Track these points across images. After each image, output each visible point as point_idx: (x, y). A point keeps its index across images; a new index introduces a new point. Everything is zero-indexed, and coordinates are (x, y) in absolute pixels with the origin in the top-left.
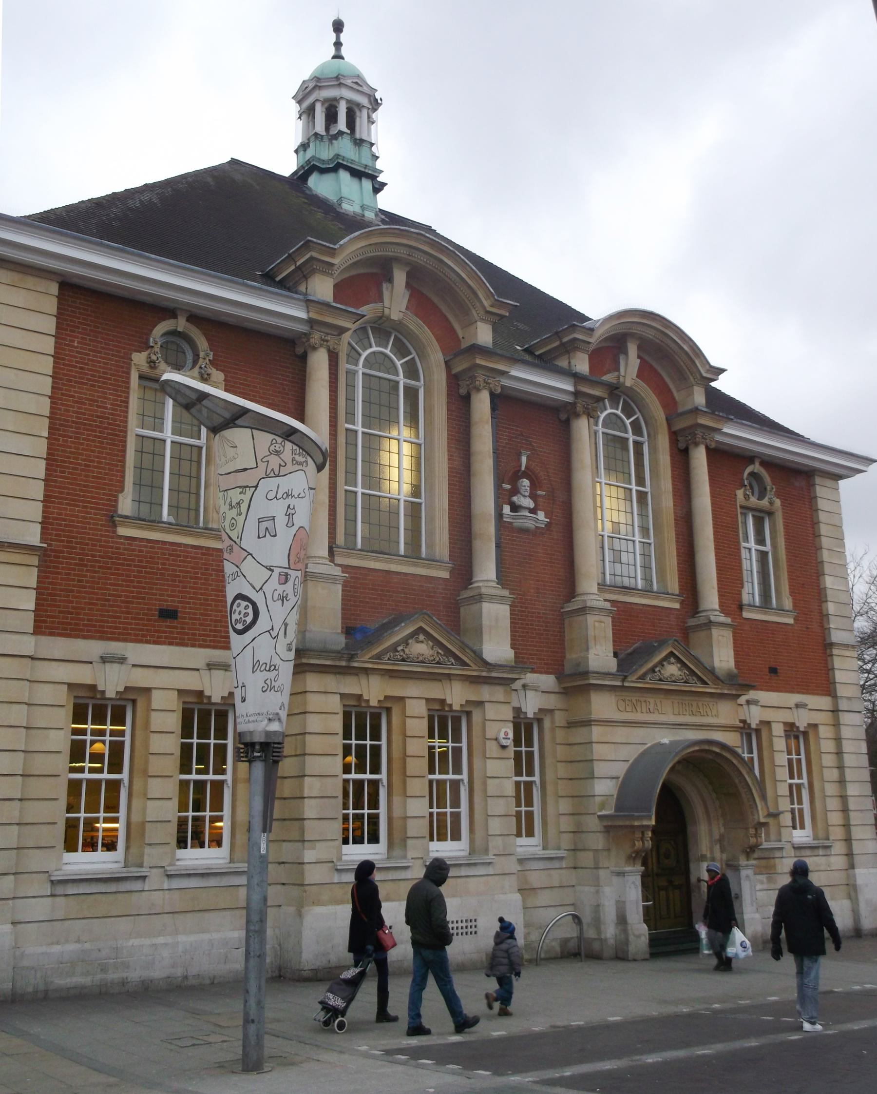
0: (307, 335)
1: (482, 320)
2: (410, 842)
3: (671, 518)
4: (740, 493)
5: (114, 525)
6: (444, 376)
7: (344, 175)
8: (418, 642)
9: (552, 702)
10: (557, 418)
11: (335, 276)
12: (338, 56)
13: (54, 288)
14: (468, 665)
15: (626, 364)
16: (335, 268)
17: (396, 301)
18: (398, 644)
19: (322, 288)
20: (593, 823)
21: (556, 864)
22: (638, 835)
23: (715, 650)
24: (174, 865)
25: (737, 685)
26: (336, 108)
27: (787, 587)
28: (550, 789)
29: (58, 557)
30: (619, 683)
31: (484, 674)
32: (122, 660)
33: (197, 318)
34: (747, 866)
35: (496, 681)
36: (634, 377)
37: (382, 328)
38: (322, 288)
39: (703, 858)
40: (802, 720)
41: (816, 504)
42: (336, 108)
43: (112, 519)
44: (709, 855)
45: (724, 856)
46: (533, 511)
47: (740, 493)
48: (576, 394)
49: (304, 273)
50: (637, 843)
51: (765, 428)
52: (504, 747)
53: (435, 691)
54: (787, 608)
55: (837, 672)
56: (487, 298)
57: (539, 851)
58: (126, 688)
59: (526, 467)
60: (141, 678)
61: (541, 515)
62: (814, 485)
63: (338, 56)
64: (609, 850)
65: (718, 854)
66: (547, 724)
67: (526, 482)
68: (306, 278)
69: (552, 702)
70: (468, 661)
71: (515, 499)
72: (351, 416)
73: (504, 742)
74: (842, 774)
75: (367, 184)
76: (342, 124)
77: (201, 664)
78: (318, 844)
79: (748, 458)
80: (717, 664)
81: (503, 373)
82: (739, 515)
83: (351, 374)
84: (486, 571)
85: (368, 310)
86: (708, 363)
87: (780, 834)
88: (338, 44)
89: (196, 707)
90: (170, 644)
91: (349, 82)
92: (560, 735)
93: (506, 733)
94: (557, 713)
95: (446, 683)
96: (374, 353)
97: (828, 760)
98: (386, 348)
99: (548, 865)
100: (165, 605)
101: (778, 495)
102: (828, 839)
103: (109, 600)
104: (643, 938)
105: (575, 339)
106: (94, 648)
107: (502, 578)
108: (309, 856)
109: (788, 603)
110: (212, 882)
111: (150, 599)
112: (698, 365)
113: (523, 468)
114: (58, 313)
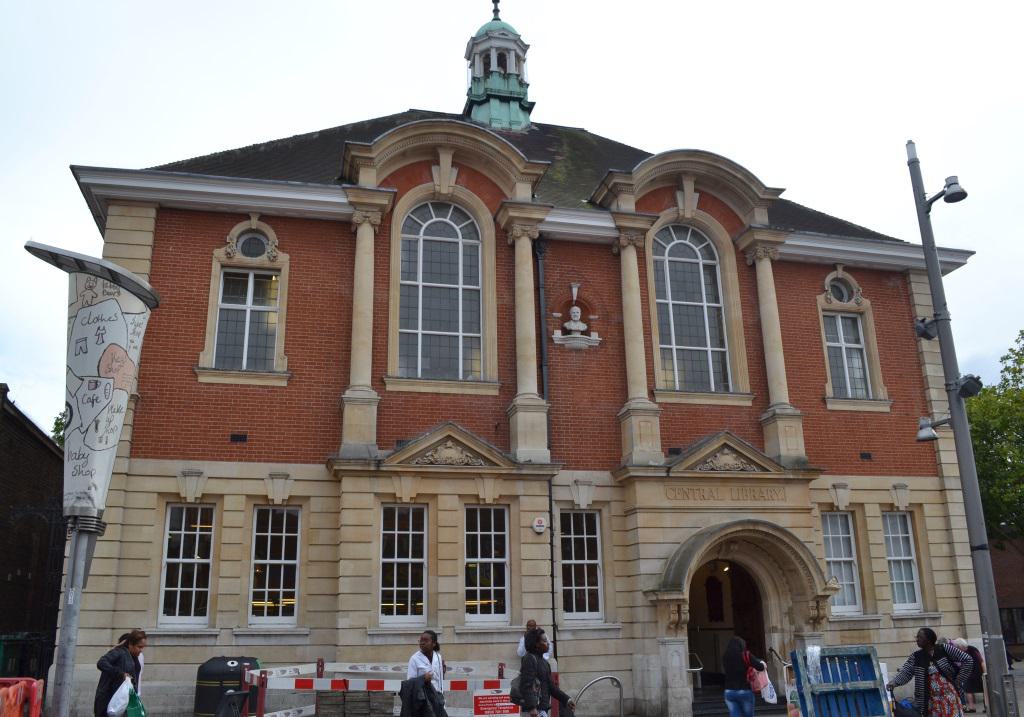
0: (618, 239)
1: (520, 181)
2: (441, 614)
3: (741, 330)
4: (821, 299)
5: (196, 375)
6: (493, 232)
7: (494, 103)
8: (447, 448)
9: (606, 494)
10: (607, 252)
11: (636, 193)
12: (496, 19)
13: (152, 213)
14: (768, 470)
15: (440, 175)
16: (376, 160)
17: (688, 203)
18: (427, 449)
19: (627, 203)
20: (640, 599)
21: (612, 635)
22: (674, 608)
23: (781, 439)
24: (378, 626)
25: (805, 471)
26: (496, 57)
27: (881, 374)
28: (608, 568)
29: (152, 402)
30: (664, 474)
31: (514, 472)
32: (199, 474)
33: (265, 217)
34: (811, 636)
35: (431, 476)
36: (695, 209)
37: (680, 227)
38: (627, 203)
39: (774, 629)
40: (902, 500)
41: (913, 300)
42: (496, 57)
43: (194, 370)
44: (779, 627)
45: (793, 628)
46: (586, 333)
47: (821, 299)
48: (619, 228)
49: (614, 193)
50: (672, 616)
51: (310, 184)
52: (539, 534)
53: (468, 487)
54: (882, 398)
55: (942, 453)
56: (520, 162)
57: (600, 624)
58: (203, 495)
59: (578, 297)
60: (215, 488)
61: (595, 336)
62: (910, 282)
63: (496, 19)
64: (656, 622)
65: (787, 626)
66: (605, 513)
67: (576, 311)
68: (616, 196)
69: (606, 494)
70: (498, 462)
71: (566, 325)
72: (661, 293)
73: (538, 529)
74: (952, 549)
75: (515, 106)
76: (494, 66)
77: (889, 486)
78: (351, 614)
79: (824, 267)
80: (783, 451)
81: (541, 221)
82: (821, 318)
83: (659, 265)
84: (528, 384)
85: (666, 216)
86: (763, 185)
87: (876, 607)
88: (496, 11)
89: (572, 513)
90: (241, 460)
91: (496, 34)
92: (616, 522)
93: (540, 522)
94: (612, 504)
95: (479, 481)
96: (677, 244)
97: (936, 537)
98: (686, 239)
99: (604, 635)
100: (236, 432)
101: (864, 295)
102: (937, 611)
103: (191, 431)
104: (685, 701)
105: (616, 184)
106: (177, 466)
107: (793, 402)
108: (343, 622)
109: (883, 393)
110: (273, 641)
111: (167, 426)
112: (755, 189)
113: (575, 298)
114: (156, 229)
